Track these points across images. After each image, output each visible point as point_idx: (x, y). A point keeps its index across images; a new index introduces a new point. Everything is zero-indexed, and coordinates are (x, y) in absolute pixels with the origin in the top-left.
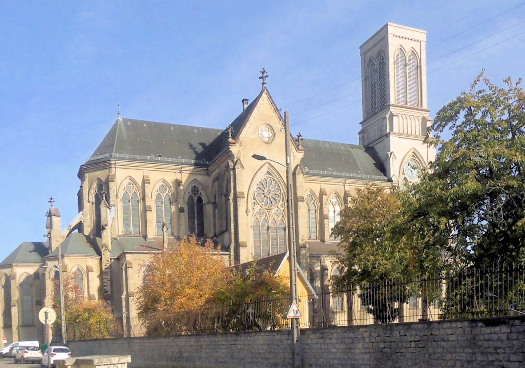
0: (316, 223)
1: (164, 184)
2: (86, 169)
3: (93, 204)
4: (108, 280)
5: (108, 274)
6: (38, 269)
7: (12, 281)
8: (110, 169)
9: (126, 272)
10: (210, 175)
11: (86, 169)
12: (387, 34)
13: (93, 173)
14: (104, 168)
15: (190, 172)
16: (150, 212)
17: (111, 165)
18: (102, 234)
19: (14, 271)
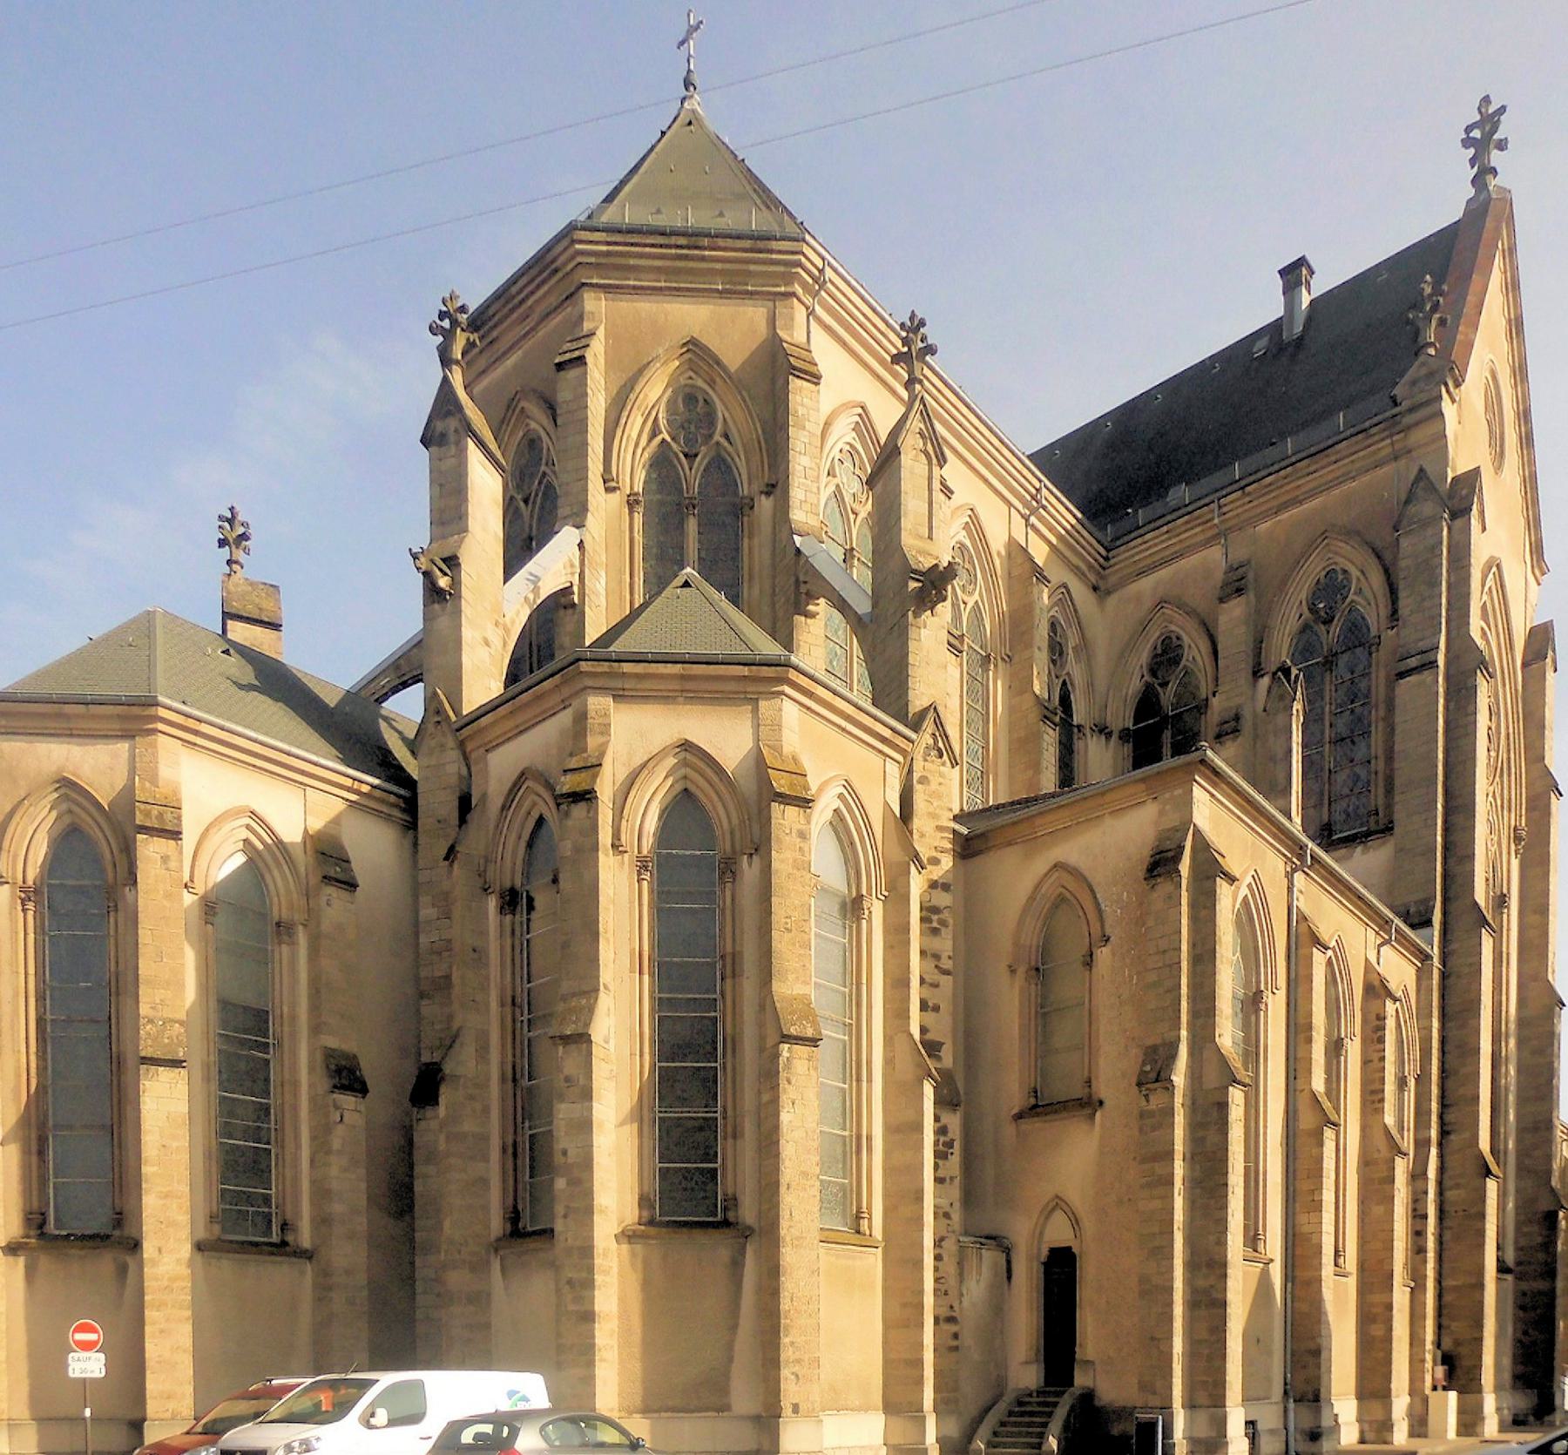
0: (1295, 1059)
1: (968, 542)
2: (603, 264)
3: (632, 503)
4: (946, 972)
5: (943, 923)
6: (336, 821)
7: (150, 850)
8: (781, 308)
9: (1285, 856)
10: (1109, 593)
11: (603, 264)
12: (900, 529)
13: (645, 307)
14: (735, 290)
15: (354, 797)
16: (344, 895)
17: (790, 278)
18: (912, 633)
19: (165, 772)
